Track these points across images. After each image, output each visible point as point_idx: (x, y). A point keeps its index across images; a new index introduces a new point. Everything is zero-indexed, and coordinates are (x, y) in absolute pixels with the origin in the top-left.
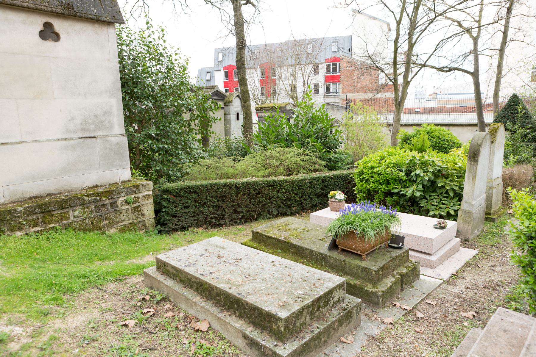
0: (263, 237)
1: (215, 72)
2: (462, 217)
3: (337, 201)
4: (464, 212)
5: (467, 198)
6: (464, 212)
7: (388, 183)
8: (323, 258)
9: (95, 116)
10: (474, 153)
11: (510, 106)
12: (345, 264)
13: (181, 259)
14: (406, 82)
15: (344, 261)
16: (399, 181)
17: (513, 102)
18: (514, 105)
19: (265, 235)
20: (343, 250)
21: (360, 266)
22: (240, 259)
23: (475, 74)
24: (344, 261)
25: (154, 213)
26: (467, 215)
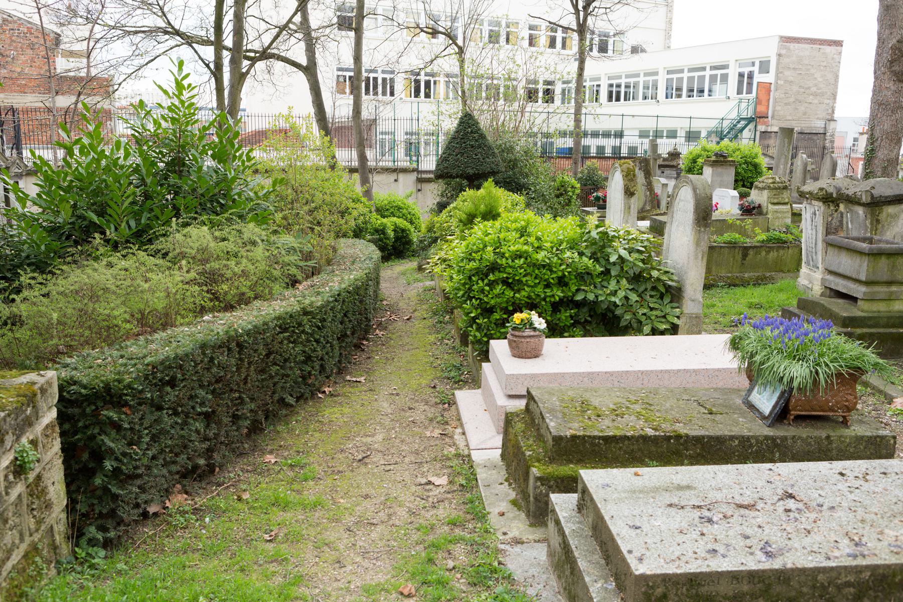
0: (593, 445)
1: (675, 43)
2: (687, 327)
3: (537, 333)
4: (690, 317)
5: (692, 293)
6: (690, 317)
7: (562, 282)
8: (776, 445)
9: (622, 132)
10: (705, 212)
11: (466, 134)
12: (830, 443)
13: (717, 548)
14: (237, 76)
15: (828, 437)
16: (584, 276)
17: (469, 127)
18: (472, 132)
19: (600, 438)
20: (798, 418)
21: (863, 436)
22: (671, 505)
23: (310, 70)
24: (828, 437)
25: (667, 428)
26: (695, 323)
